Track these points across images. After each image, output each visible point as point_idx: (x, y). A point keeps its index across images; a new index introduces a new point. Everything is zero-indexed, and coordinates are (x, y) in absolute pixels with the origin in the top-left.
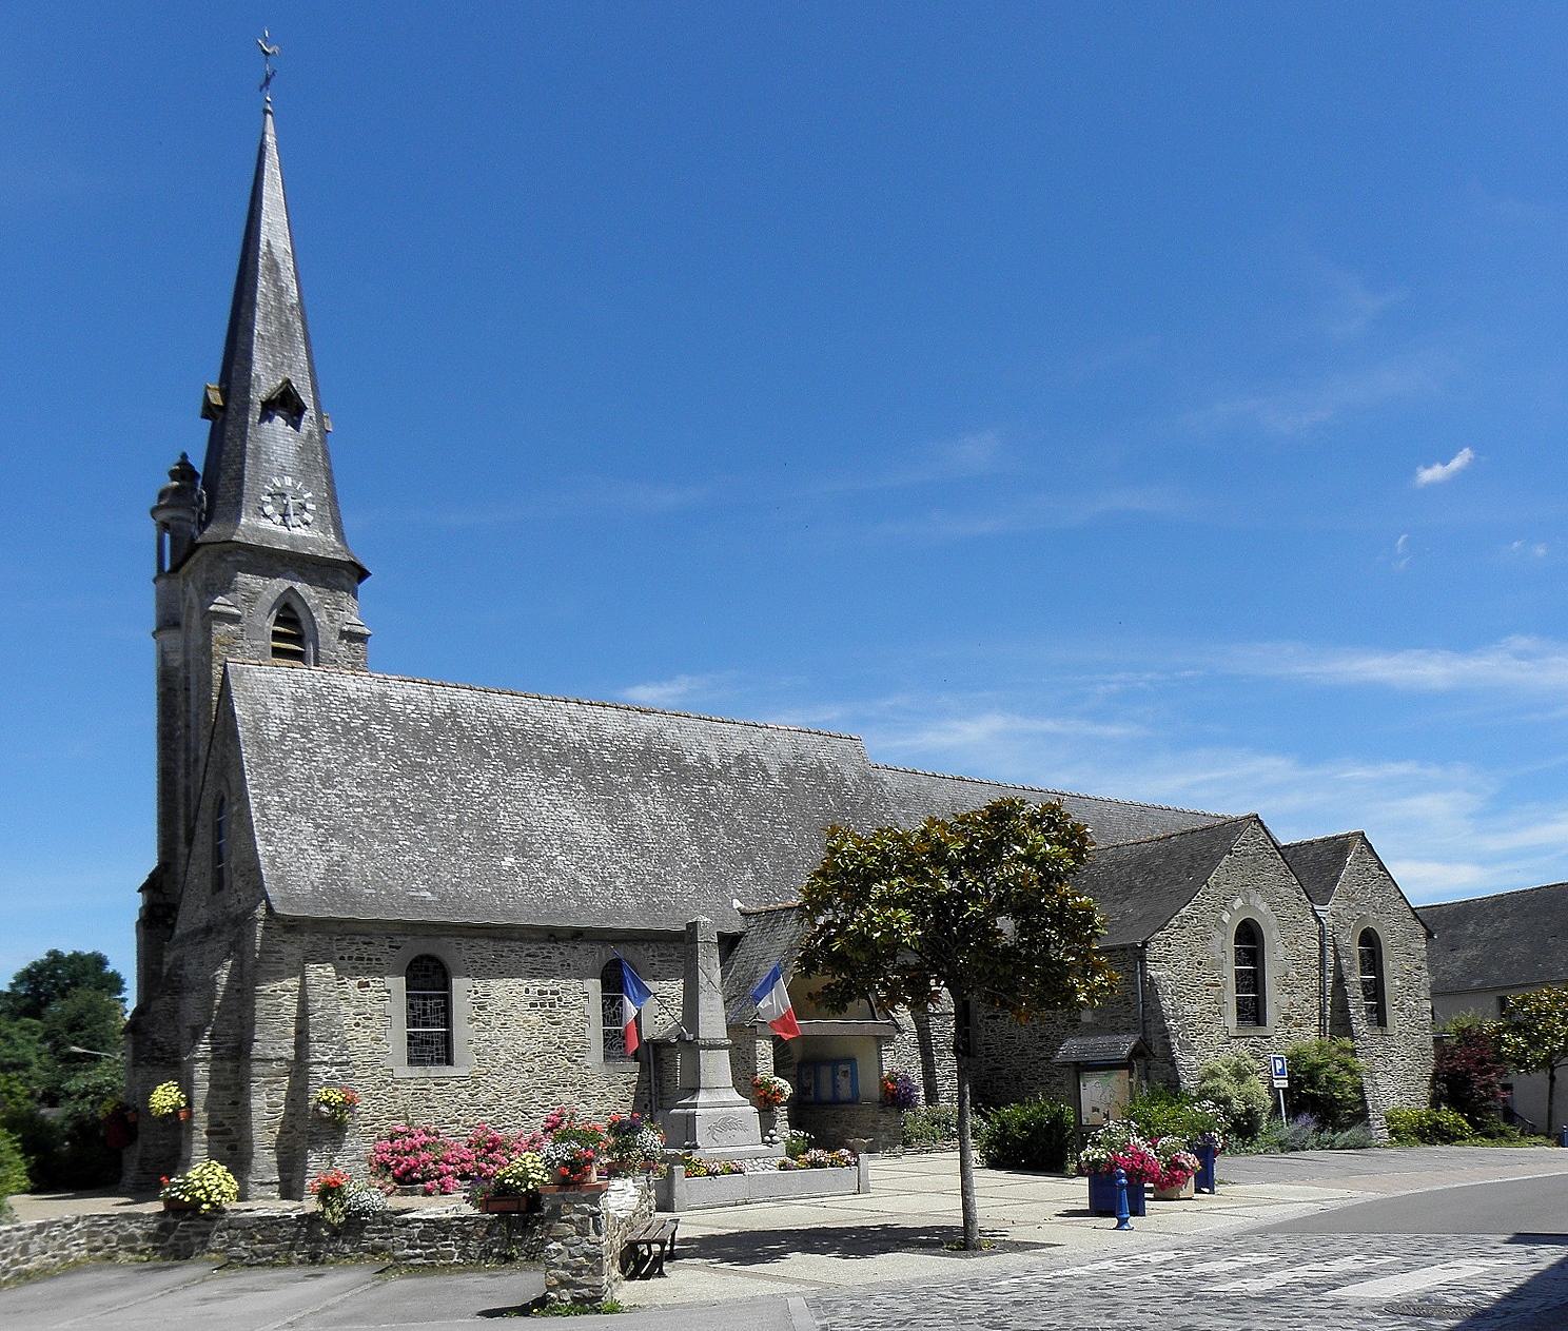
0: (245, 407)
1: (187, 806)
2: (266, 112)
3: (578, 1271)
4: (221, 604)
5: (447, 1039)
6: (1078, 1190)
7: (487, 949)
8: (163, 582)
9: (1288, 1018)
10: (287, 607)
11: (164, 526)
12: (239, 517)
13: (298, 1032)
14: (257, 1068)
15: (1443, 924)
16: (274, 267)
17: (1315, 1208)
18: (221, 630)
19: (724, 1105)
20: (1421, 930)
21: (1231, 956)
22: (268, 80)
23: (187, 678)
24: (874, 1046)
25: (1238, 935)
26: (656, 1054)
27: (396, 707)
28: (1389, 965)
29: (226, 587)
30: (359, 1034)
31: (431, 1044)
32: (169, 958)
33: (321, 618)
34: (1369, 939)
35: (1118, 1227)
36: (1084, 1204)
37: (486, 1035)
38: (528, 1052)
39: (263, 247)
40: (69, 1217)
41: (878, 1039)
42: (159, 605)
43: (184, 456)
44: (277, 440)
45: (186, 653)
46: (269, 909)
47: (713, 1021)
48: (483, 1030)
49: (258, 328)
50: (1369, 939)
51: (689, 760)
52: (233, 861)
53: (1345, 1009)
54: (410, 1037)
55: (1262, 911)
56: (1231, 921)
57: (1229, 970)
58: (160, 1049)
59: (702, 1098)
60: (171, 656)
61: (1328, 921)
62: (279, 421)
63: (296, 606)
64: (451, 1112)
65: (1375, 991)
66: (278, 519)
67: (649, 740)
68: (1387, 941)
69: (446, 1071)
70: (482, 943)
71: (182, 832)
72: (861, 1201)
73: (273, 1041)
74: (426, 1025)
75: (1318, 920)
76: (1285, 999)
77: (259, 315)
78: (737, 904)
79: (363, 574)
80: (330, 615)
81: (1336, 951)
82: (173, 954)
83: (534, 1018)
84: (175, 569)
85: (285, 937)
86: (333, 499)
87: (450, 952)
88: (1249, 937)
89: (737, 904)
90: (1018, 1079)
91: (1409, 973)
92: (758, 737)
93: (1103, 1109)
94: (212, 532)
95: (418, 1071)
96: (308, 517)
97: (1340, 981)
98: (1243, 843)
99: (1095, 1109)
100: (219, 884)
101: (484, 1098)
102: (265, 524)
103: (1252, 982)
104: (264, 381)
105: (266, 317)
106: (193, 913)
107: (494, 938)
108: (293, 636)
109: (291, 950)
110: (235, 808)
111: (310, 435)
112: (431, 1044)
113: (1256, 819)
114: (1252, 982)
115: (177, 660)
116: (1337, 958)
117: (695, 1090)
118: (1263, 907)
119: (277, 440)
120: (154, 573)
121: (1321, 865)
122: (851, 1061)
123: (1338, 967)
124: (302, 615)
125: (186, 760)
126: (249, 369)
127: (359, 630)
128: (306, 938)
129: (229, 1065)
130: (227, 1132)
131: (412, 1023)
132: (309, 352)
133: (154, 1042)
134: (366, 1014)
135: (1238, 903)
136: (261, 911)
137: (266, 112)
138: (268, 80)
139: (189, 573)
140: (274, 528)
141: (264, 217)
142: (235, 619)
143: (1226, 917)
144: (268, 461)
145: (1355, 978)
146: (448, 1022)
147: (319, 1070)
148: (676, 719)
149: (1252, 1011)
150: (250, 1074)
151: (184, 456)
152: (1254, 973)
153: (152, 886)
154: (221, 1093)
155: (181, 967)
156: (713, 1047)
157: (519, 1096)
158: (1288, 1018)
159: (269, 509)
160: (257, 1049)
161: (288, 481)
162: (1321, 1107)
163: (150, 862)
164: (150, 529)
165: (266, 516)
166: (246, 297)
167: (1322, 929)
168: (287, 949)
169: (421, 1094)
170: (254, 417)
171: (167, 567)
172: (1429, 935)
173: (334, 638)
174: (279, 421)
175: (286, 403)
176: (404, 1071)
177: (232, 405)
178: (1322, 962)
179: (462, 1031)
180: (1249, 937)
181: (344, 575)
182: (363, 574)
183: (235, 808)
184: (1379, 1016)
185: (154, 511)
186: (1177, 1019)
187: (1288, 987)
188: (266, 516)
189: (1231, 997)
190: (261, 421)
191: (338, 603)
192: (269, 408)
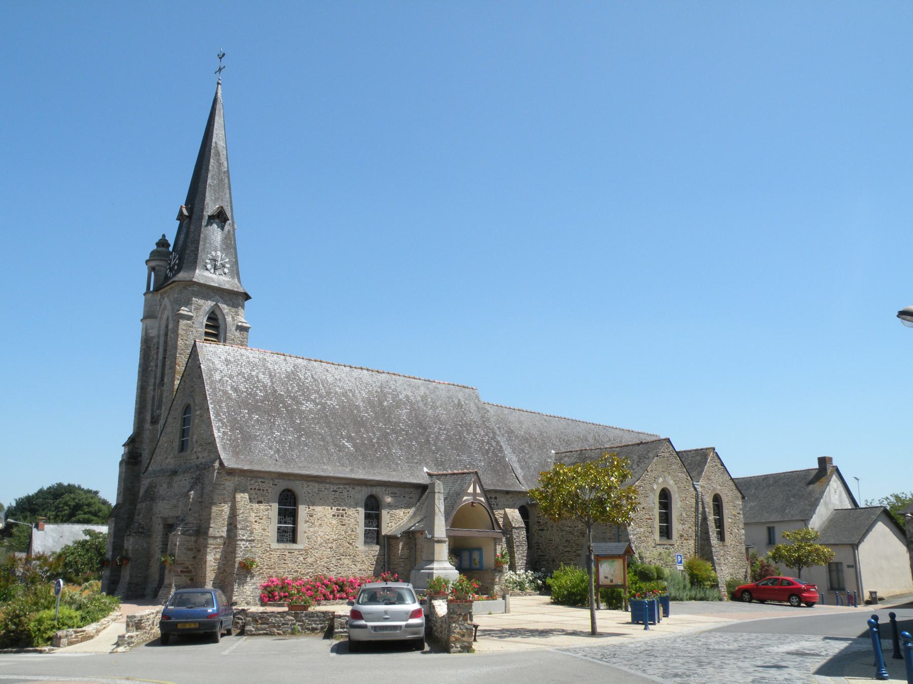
0: (201, 218)
1: (153, 405)
2: (218, 84)
3: (463, 636)
4: (184, 311)
5: (294, 531)
6: (627, 616)
7: (316, 486)
8: (150, 295)
9: (682, 536)
10: (213, 312)
11: (153, 269)
12: (195, 269)
13: (230, 524)
14: (210, 541)
15: (744, 486)
16: (218, 154)
17: (726, 624)
18: (183, 323)
19: (445, 569)
20: (739, 495)
21: (657, 505)
22: (220, 69)
23: (158, 343)
24: (492, 545)
25: (660, 495)
26: (389, 545)
27: (270, 366)
28: (726, 512)
29: (188, 303)
30: (256, 526)
31: (288, 535)
32: (145, 483)
33: (229, 319)
34: (717, 499)
35: (645, 629)
36: (630, 620)
37: (311, 529)
38: (332, 538)
39: (213, 144)
40: (154, 611)
41: (495, 539)
42: (145, 306)
43: (164, 236)
44: (215, 234)
45: (159, 331)
46: (221, 464)
47: (440, 529)
48: (311, 527)
49: (209, 181)
50: (717, 499)
51: (401, 397)
52: (194, 437)
53: (707, 533)
54: (279, 529)
55: (671, 485)
56: (657, 488)
57: (656, 511)
58: (143, 528)
59: (435, 565)
60: (150, 331)
61: (699, 489)
62: (215, 226)
63: (218, 312)
64: (294, 566)
65: (720, 524)
66: (212, 271)
67: (381, 387)
68: (725, 499)
69: (294, 546)
70: (314, 484)
71: (148, 418)
72: (506, 616)
73: (218, 528)
74: (285, 523)
75: (695, 489)
76: (680, 527)
77: (209, 176)
78: (425, 470)
79: (247, 297)
80: (233, 318)
81: (703, 504)
82: (148, 480)
83: (334, 522)
84: (156, 290)
85: (227, 477)
86: (236, 263)
87: (300, 489)
88: (665, 497)
89: (425, 470)
90: (554, 561)
91: (735, 516)
92: (431, 386)
93: (610, 577)
94: (182, 276)
95: (282, 546)
96: (226, 270)
97: (705, 519)
98: (664, 451)
99: (606, 577)
100: (183, 447)
101: (310, 560)
102: (207, 273)
103: (666, 517)
104: (211, 208)
105: (212, 177)
106: (164, 458)
107: (318, 482)
108: (215, 329)
109: (230, 483)
110: (198, 413)
111: (229, 231)
112: (288, 535)
113: (668, 440)
114: (666, 517)
115: (153, 333)
116: (703, 508)
117: (432, 561)
118: (671, 482)
119: (215, 234)
120: (145, 291)
121: (696, 461)
122: (480, 549)
123: (704, 512)
124: (220, 317)
125: (155, 383)
126: (204, 200)
127: (245, 325)
128: (236, 478)
129: (193, 538)
130: (189, 572)
131: (280, 522)
132: (230, 193)
133: (140, 524)
134: (259, 519)
135: (661, 480)
136: (217, 465)
137: (218, 84)
138: (220, 69)
139: (165, 292)
140: (210, 275)
141: (215, 132)
142: (190, 318)
143: (655, 487)
144: (210, 244)
145: (711, 518)
146: (295, 522)
147: (241, 543)
148: (394, 377)
149: (666, 532)
150: (207, 544)
151: (164, 236)
152: (666, 514)
153: (133, 444)
154: (189, 552)
155: (155, 487)
156: (439, 542)
157: (326, 560)
158: (682, 536)
159: (209, 266)
160: (211, 532)
161: (219, 253)
162: (699, 585)
163: (128, 430)
164: (145, 270)
165: (207, 269)
166: (204, 167)
167: (697, 494)
168: (227, 483)
169: (282, 557)
170: (204, 223)
171: (151, 289)
172: (743, 498)
173: (234, 328)
174: (215, 226)
175: (221, 217)
176: (275, 545)
177: (194, 216)
178: (697, 509)
179: (302, 526)
180: (665, 497)
181: (238, 298)
182: (247, 297)
183: (198, 413)
184: (721, 537)
185: (147, 262)
186: (634, 535)
187: (682, 521)
188: (207, 269)
189: (657, 524)
190: (207, 225)
191: (237, 312)
192: (211, 218)
